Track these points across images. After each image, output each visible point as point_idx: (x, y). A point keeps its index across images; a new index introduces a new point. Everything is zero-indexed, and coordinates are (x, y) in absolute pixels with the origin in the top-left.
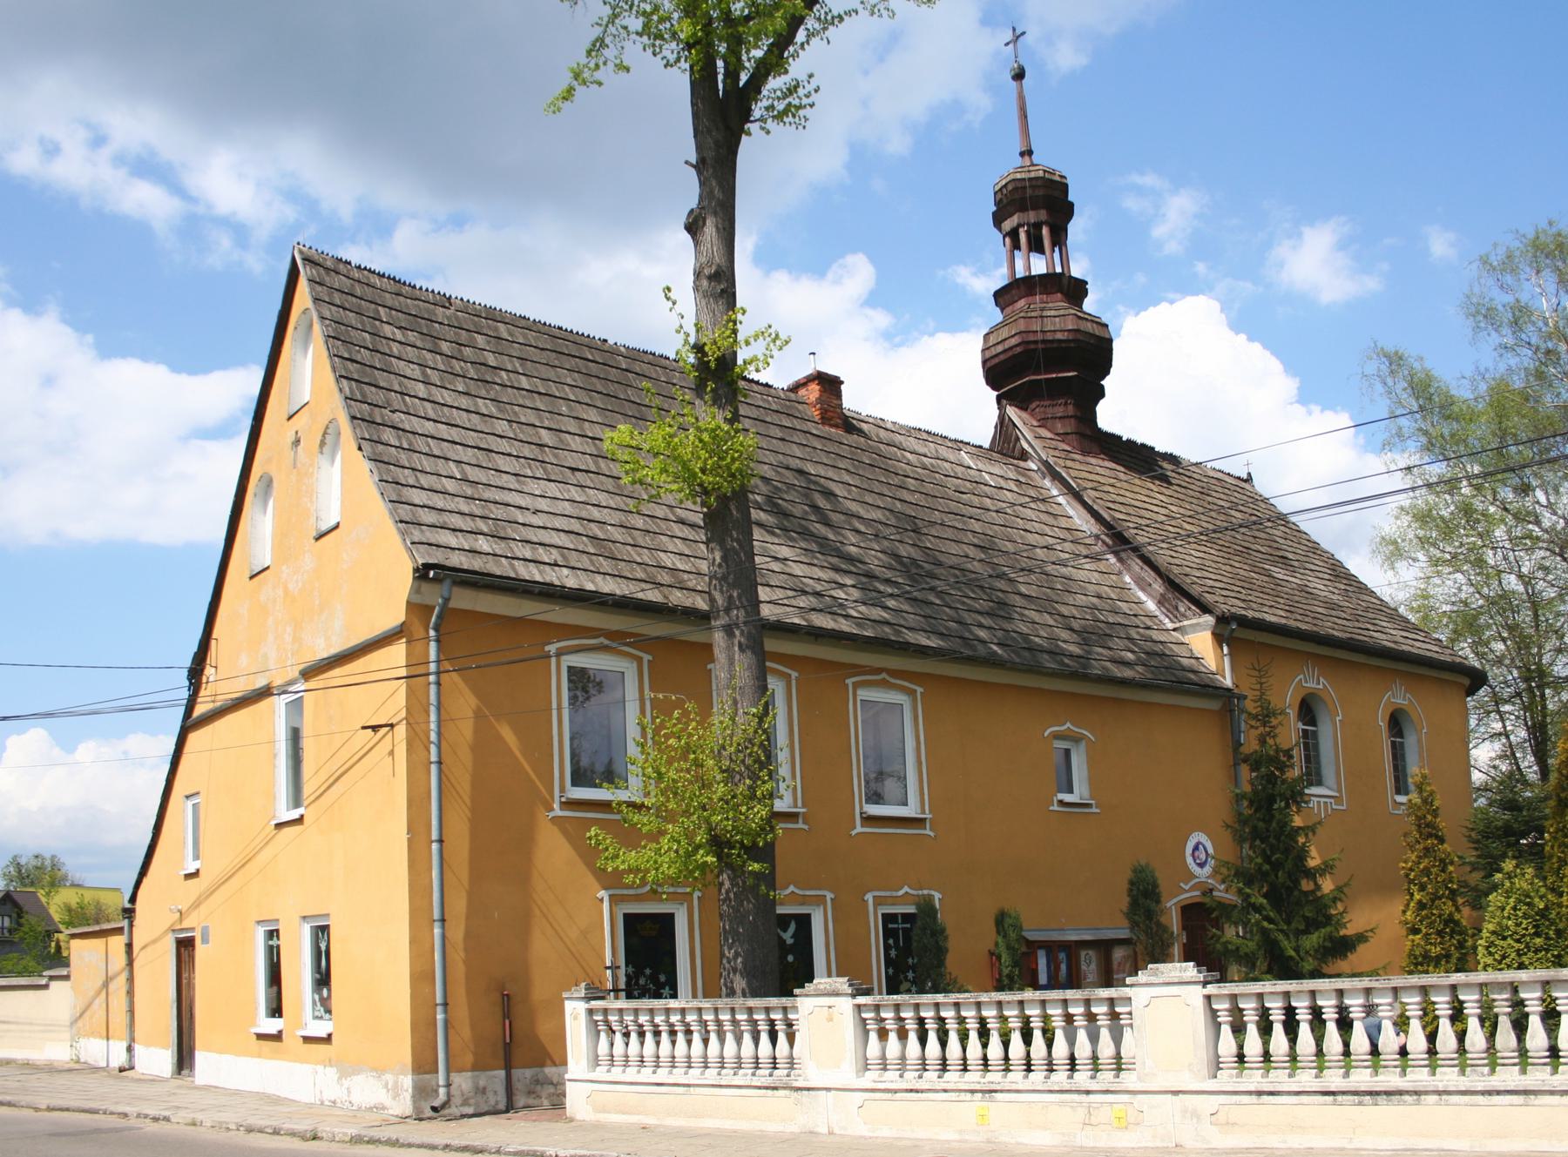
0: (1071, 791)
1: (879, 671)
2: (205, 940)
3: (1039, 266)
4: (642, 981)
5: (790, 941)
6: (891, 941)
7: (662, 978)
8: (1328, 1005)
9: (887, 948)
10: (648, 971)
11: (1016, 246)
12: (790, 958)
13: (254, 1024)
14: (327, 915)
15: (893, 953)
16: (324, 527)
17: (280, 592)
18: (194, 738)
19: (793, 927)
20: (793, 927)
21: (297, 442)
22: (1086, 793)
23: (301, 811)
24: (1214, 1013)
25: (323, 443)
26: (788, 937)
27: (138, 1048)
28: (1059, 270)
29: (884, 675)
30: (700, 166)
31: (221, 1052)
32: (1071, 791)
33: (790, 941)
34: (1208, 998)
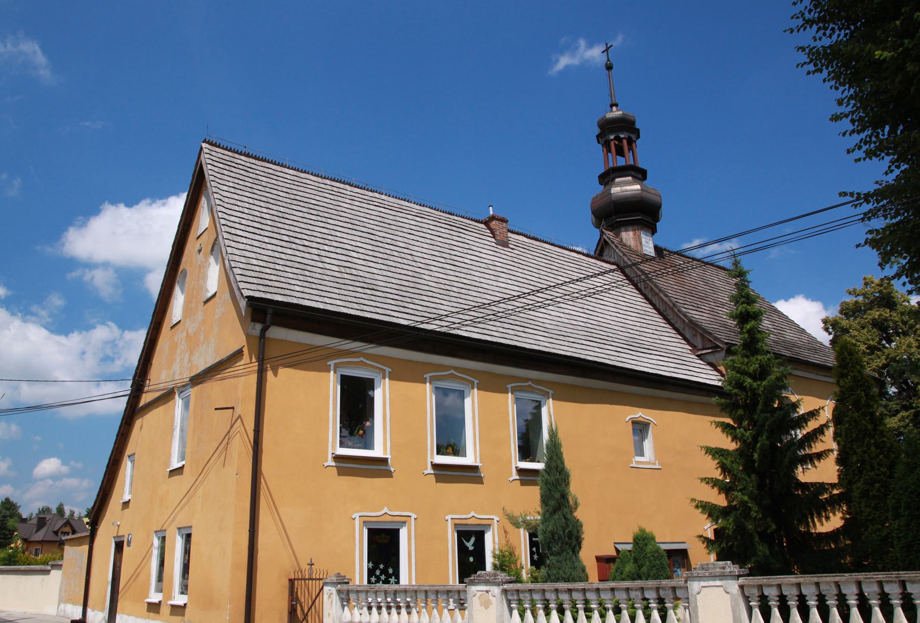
0: (642, 455)
1: (527, 380)
2: (129, 545)
3: (621, 162)
4: (378, 572)
5: (471, 548)
6: (534, 549)
7: (391, 571)
8: (851, 592)
9: (532, 553)
10: (382, 566)
11: (609, 150)
12: (471, 559)
13: (147, 597)
14: (191, 527)
15: (536, 557)
16: (210, 295)
17: (185, 335)
18: (140, 424)
19: (473, 539)
20: (473, 539)
21: (200, 251)
22: (653, 458)
23: (183, 463)
24: (747, 599)
25: (212, 250)
26: (470, 545)
27: (89, 610)
28: (632, 163)
29: (530, 383)
30: (560, 445)
31: (129, 615)
32: (642, 455)
33: (471, 548)
34: (742, 587)
